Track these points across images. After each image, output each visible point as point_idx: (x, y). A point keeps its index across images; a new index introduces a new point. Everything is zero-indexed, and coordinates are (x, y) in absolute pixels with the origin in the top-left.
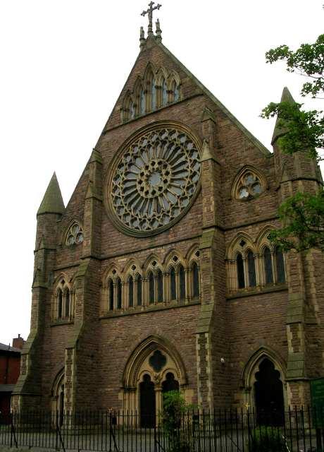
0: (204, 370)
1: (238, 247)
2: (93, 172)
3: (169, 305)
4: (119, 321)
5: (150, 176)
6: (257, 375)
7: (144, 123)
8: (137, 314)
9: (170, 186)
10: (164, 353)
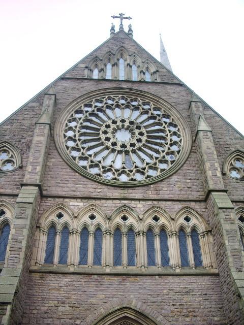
1: (53, 218)
2: (182, 83)
3: (144, 271)
4: (66, 280)
5: (120, 129)
7: (115, 85)
9: (134, 152)
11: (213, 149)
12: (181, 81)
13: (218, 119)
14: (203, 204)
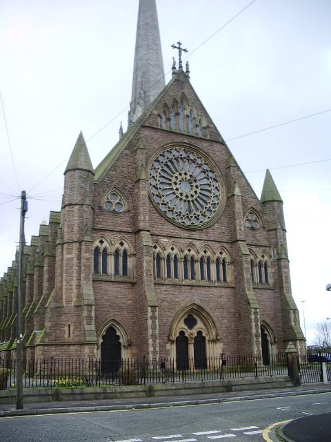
0: (257, 331)
4: (164, 288)
6: (118, 337)
8: (180, 285)
10: (195, 317)
11: (241, 209)
12: (223, 140)
13: (243, 179)
14: (230, 245)
